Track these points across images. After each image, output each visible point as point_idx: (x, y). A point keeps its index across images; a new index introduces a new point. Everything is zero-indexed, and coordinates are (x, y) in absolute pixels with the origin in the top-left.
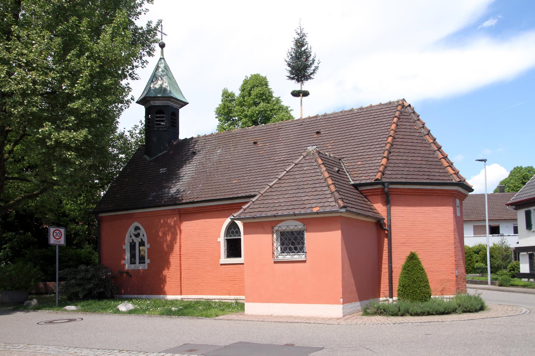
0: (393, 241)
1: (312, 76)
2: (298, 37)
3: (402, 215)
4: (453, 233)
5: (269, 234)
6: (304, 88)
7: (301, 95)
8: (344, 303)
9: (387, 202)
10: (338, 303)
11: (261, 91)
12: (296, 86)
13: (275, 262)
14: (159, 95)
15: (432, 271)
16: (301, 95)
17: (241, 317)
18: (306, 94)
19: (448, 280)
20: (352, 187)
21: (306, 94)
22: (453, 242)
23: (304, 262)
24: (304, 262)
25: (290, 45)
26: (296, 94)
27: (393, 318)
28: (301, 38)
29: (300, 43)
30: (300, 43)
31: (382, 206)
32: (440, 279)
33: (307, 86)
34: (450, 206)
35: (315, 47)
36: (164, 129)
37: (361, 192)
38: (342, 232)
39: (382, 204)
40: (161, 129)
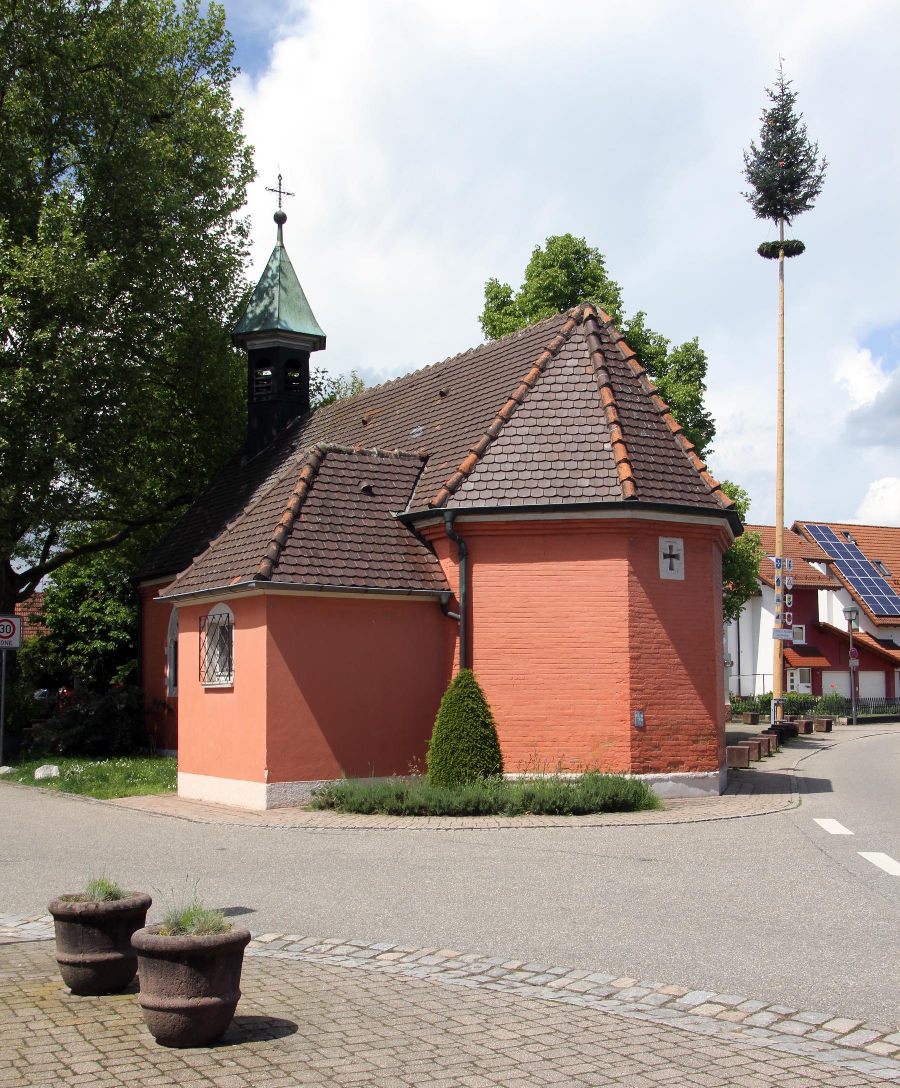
0: (477, 644)
1: (809, 202)
2: (775, 105)
3: (501, 584)
4: (627, 624)
5: (190, 631)
6: (790, 235)
7: (781, 253)
8: (269, 781)
9: (466, 559)
10: (260, 781)
11: (544, 281)
12: (770, 231)
13: (208, 691)
14: (256, 330)
15: (572, 715)
16: (781, 253)
17: (168, 802)
18: (794, 249)
19: (612, 738)
20: (397, 524)
21: (794, 249)
22: (628, 644)
23: (230, 690)
24: (230, 690)
25: (752, 135)
26: (770, 251)
27: (394, 818)
28: (783, 107)
29: (780, 124)
30: (780, 124)
31: (452, 564)
32: (592, 733)
33: (798, 228)
34: (621, 557)
35: (815, 127)
36: (270, 398)
37: (419, 536)
38: (272, 631)
39: (453, 560)
40: (265, 399)
